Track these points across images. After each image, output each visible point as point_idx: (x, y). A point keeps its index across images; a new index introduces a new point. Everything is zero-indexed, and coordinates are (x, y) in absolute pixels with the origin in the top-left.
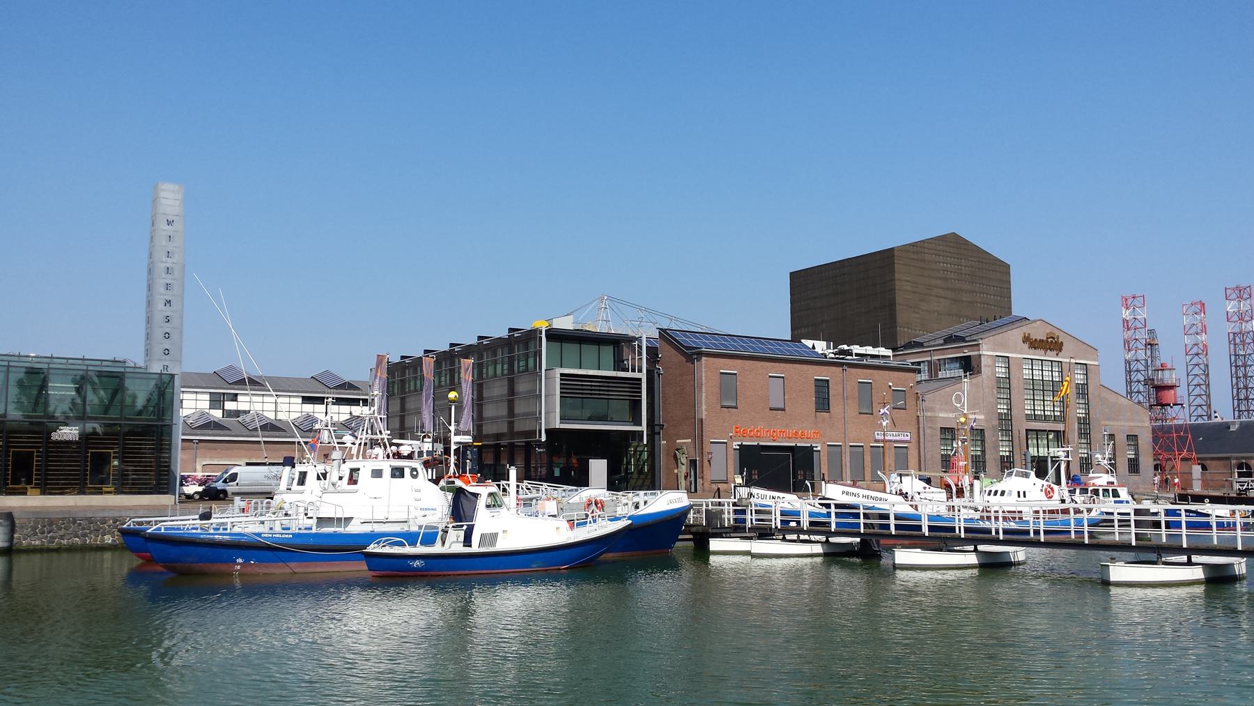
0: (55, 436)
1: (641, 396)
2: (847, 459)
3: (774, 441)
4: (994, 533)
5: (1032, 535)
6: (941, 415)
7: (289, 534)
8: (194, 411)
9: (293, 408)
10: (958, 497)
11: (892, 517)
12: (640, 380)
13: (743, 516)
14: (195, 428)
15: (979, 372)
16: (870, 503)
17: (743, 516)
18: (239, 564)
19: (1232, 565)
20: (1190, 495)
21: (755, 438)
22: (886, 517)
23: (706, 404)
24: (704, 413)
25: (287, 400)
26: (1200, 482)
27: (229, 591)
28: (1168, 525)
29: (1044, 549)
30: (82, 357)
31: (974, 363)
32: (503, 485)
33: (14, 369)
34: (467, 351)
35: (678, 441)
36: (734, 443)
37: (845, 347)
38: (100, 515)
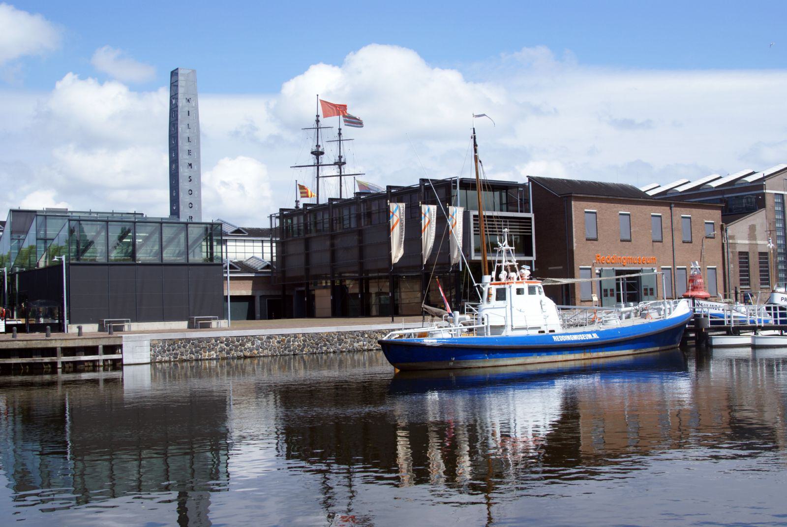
1: (531, 232)
3: (624, 266)
4: (757, 322)
5: (757, 322)
7: (591, 333)
10: (497, 299)
12: (530, 219)
18: (692, 338)
19: (635, 351)
20: (11, 244)
21: (611, 264)
23: (575, 238)
25: (234, 244)
26: (269, 227)
28: (473, 319)
29: (495, 345)
30: (134, 212)
32: (467, 306)
34: (398, 194)
35: (550, 268)
36: (596, 268)
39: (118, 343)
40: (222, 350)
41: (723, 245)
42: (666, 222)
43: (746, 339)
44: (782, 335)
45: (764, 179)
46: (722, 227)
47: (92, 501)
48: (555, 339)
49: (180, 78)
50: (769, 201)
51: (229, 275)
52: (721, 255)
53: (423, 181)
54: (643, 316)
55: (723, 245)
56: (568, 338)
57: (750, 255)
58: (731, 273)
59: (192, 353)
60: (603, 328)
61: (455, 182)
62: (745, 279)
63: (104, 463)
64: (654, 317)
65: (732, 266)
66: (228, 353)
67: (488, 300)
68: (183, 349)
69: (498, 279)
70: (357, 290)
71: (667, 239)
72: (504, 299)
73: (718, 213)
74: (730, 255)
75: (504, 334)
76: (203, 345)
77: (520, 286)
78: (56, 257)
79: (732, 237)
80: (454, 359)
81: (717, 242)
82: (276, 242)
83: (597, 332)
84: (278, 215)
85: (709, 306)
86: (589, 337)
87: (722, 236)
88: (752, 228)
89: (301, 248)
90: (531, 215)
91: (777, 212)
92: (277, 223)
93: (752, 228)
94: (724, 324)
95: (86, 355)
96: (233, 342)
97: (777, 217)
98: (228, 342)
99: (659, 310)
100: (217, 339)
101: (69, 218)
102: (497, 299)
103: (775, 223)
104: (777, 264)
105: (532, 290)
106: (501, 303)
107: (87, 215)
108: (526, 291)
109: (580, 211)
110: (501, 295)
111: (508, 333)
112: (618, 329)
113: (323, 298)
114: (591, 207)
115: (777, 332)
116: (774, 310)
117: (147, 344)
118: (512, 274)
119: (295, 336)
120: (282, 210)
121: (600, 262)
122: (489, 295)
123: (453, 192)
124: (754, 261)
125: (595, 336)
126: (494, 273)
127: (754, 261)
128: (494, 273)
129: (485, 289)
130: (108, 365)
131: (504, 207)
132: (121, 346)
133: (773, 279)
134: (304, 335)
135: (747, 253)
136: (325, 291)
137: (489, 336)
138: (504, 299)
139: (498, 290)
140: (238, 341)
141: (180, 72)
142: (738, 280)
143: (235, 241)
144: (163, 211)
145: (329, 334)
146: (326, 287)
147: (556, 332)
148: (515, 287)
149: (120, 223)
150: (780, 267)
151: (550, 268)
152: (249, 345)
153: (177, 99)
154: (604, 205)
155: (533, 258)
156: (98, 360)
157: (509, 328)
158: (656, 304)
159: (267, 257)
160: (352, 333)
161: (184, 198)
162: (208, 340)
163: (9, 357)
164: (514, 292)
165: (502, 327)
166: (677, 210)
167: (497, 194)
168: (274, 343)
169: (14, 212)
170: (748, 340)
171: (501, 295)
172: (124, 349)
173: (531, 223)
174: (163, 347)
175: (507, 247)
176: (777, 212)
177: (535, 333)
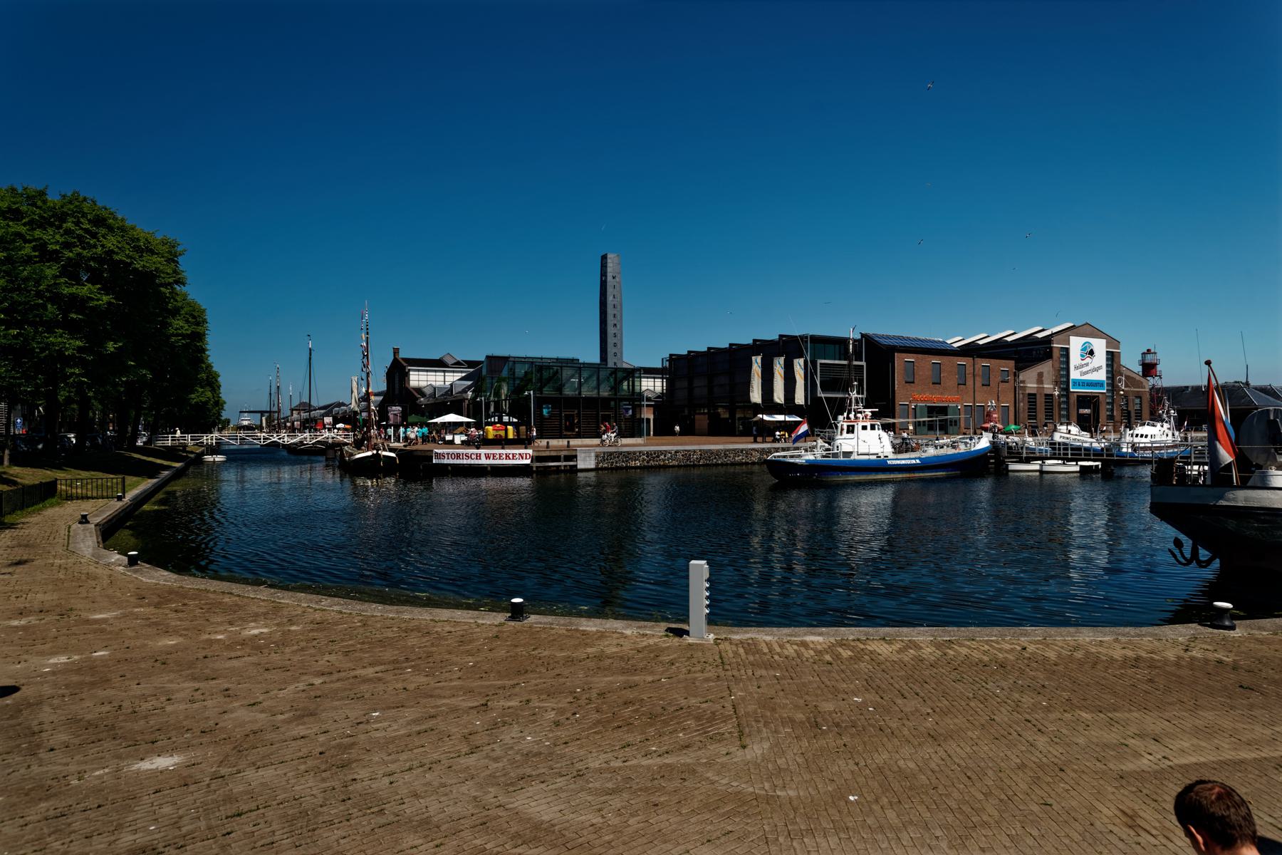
7: (915, 459)
10: (848, 432)
18: (992, 463)
26: (660, 366)
40: (644, 460)
41: (1015, 387)
42: (969, 370)
43: (1035, 466)
44: (1064, 463)
45: (1052, 335)
46: (1015, 373)
48: (889, 462)
49: (609, 261)
50: (1056, 354)
51: (645, 403)
52: (1013, 395)
53: (781, 336)
54: (954, 447)
55: (1015, 387)
56: (898, 462)
57: (1038, 396)
58: (1021, 410)
59: (623, 462)
60: (924, 455)
61: (807, 337)
62: (1032, 416)
63: (1157, 527)
64: (962, 448)
65: (1022, 404)
66: (648, 462)
67: (841, 434)
68: (617, 459)
69: (848, 418)
70: (727, 416)
71: (970, 382)
72: (853, 432)
73: (1012, 363)
74: (1021, 396)
75: (852, 458)
76: (630, 456)
77: (864, 424)
79: (1023, 382)
81: (1009, 386)
82: (666, 378)
83: (919, 458)
86: (914, 462)
87: (1015, 380)
88: (1040, 375)
89: (685, 384)
90: (863, 363)
91: (1061, 362)
92: (666, 364)
93: (1040, 375)
96: (651, 454)
97: (1062, 366)
98: (648, 454)
99: (966, 444)
100: (640, 452)
102: (848, 432)
103: (1059, 371)
104: (1060, 404)
105: (873, 427)
106: (850, 436)
107: (539, 360)
108: (869, 427)
109: (901, 360)
110: (851, 430)
111: (854, 457)
112: (935, 456)
113: (702, 420)
114: (910, 358)
115: (1060, 462)
117: (593, 454)
118: (859, 415)
119: (695, 451)
120: (671, 355)
121: (915, 400)
122: (842, 430)
124: (1041, 401)
125: (918, 461)
126: (845, 414)
127: (1041, 401)
128: (845, 414)
129: (839, 425)
131: (842, 357)
132: (576, 456)
133: (1056, 416)
134: (700, 450)
135: (1035, 395)
136: (702, 416)
137: (842, 459)
138: (853, 432)
139: (848, 426)
141: (609, 256)
142: (1026, 416)
144: (596, 359)
145: (718, 451)
146: (704, 414)
147: (890, 457)
148: (861, 424)
150: (1062, 406)
152: (662, 457)
153: (606, 276)
154: (920, 356)
155: (865, 396)
157: (856, 454)
158: (963, 438)
159: (659, 389)
160: (734, 450)
161: (611, 350)
162: (634, 453)
164: (860, 428)
165: (851, 453)
166: (978, 360)
167: (837, 346)
168: (680, 456)
169: (487, 357)
170: (1037, 467)
171: (851, 430)
172: (578, 458)
174: (603, 457)
176: (1061, 362)
177: (874, 457)
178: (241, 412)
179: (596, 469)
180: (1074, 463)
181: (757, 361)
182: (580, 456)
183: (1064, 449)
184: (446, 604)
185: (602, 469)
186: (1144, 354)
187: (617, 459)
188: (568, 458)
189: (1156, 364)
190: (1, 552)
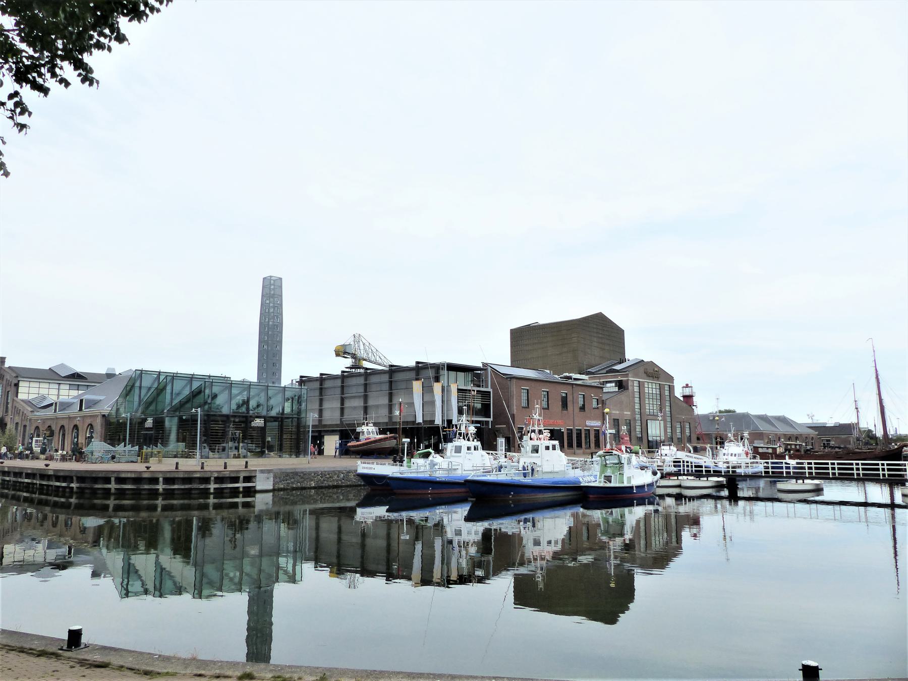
0: (253, 424)
1: (490, 402)
2: (583, 436)
6: (613, 412)
8: (37, 395)
9: (32, 390)
11: (704, 467)
12: (490, 392)
13: (680, 464)
14: (40, 408)
15: (628, 389)
16: (696, 461)
17: (680, 464)
22: (701, 467)
24: (515, 411)
27: (198, 531)
31: (624, 384)
33: (216, 384)
35: (496, 426)
37: (567, 374)
38: (308, 470)
39: (253, 475)
47: (167, 596)
78: (194, 409)
80: (431, 489)
84: (299, 380)
85: (331, 443)
94: (769, 474)
95: (231, 483)
101: (204, 380)
116: (884, 468)
123: (441, 372)
130: (37, 488)
140: (329, 474)
143: (86, 387)
149: (241, 386)
151: (496, 426)
152: (336, 477)
155: (491, 420)
156: (239, 487)
163: (125, 484)
173: (490, 395)
175: (538, 417)
178: (690, 423)
179: (273, 490)
180: (676, 478)
181: (417, 386)
182: (260, 477)
183: (688, 466)
184: (139, 653)
185: (280, 490)
186: (683, 387)
187: (292, 480)
188: (248, 479)
189: (104, 416)
190: (4, 99)
